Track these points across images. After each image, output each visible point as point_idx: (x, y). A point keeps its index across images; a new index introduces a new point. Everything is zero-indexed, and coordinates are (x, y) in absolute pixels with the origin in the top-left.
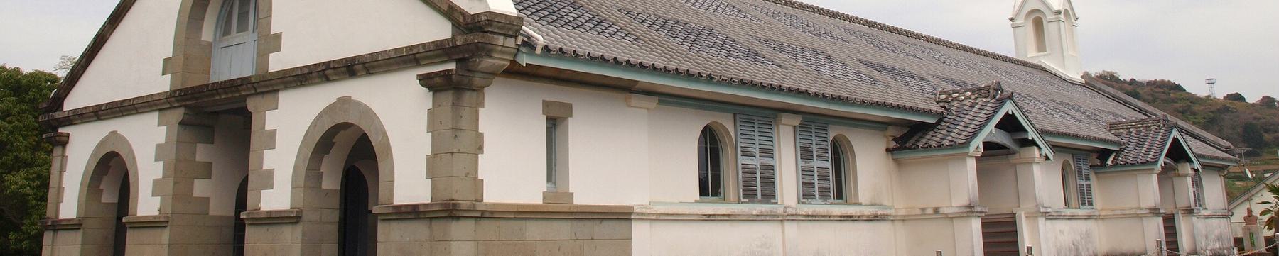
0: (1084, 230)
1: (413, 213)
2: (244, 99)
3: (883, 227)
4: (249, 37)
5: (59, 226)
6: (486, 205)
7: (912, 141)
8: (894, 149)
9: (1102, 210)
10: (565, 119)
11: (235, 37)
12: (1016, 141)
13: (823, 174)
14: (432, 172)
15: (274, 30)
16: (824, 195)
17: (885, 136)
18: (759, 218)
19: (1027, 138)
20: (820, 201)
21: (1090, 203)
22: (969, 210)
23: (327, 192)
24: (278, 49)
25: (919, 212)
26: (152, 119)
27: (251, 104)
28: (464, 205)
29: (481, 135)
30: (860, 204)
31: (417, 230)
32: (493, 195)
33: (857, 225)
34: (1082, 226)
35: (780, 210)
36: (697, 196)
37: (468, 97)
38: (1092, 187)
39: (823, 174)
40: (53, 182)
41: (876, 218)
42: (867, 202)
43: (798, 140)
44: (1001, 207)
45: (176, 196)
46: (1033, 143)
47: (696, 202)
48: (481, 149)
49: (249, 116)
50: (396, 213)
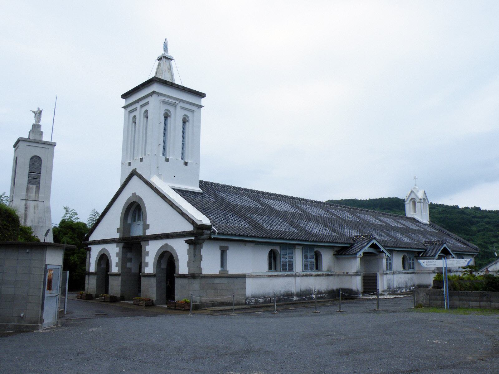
0: (410, 277)
1: (183, 276)
2: (140, 242)
3: (331, 278)
4: (141, 223)
5: (90, 274)
6: (203, 275)
7: (341, 252)
8: (336, 254)
9: (418, 270)
10: (227, 250)
11: (137, 223)
12: (378, 251)
13: (311, 263)
14: (189, 266)
15: (147, 223)
16: (311, 269)
17: (333, 250)
18: (287, 276)
19: (381, 251)
20: (310, 271)
21: (413, 268)
22: (356, 274)
23: (163, 269)
24: (149, 228)
25: (342, 273)
26: (115, 245)
27: (142, 243)
28: (197, 274)
29: (202, 256)
30: (323, 271)
31: (185, 281)
32: (205, 272)
33: (322, 278)
34: (409, 276)
35: (294, 273)
36: (267, 270)
37: (198, 246)
38: (415, 263)
39: (311, 263)
40: (87, 261)
41: (328, 275)
42: (326, 270)
43: (303, 253)
44: (371, 271)
45: (122, 268)
46: (383, 252)
47: (267, 272)
48: (202, 260)
49: (141, 247)
50: (180, 276)
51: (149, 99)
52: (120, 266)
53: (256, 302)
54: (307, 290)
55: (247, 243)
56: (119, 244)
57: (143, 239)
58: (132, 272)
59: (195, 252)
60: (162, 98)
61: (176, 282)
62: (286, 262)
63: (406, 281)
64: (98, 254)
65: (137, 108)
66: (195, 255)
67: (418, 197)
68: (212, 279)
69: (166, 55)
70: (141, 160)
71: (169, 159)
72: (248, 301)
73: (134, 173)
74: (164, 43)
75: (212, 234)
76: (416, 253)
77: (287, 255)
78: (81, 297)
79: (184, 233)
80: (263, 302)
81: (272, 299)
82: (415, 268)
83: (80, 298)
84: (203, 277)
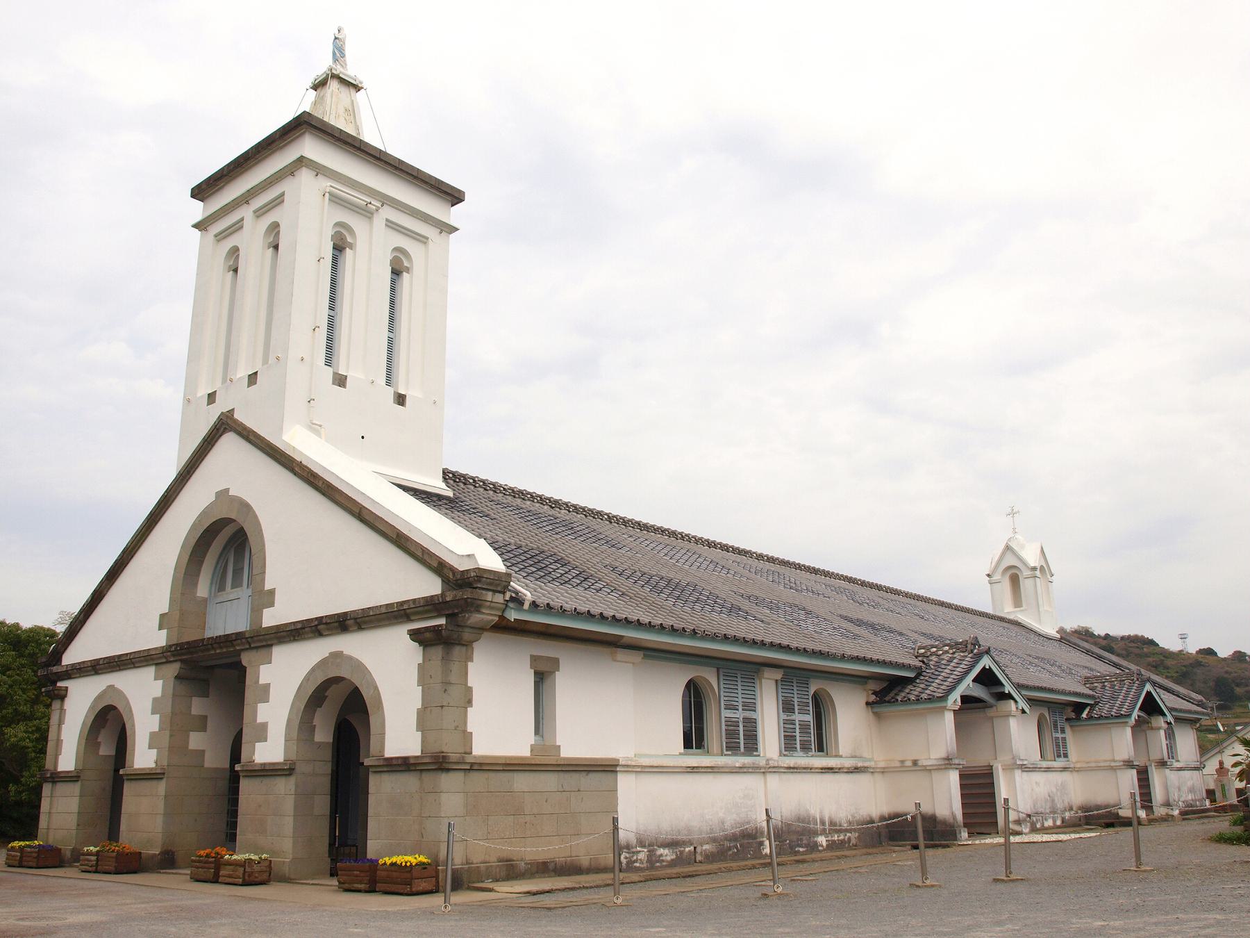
1: (404, 765)
2: (238, 653)
4: (244, 593)
6: (475, 757)
7: (892, 694)
8: (873, 703)
9: (1077, 762)
10: (552, 673)
11: (231, 593)
13: (804, 727)
14: (422, 725)
15: (268, 587)
16: (805, 748)
19: (1004, 692)
21: (1066, 756)
22: (947, 763)
23: (320, 745)
24: (272, 604)
25: (898, 764)
26: (150, 672)
27: (245, 659)
28: (454, 757)
29: (470, 689)
30: (841, 757)
31: (408, 782)
32: (482, 748)
33: (837, 776)
36: (681, 749)
37: (457, 651)
38: (1067, 739)
39: (804, 727)
40: (52, 735)
41: (856, 770)
43: (780, 694)
44: (979, 759)
46: (1010, 696)
47: (681, 754)
48: (470, 702)
49: (243, 670)
50: (387, 766)
51: (286, 186)
53: (652, 859)
54: (799, 819)
55: (619, 649)
56: (164, 667)
57: (250, 644)
58: (207, 765)
59: (446, 671)
60: (326, 184)
61: (372, 789)
63: (1051, 795)
64: (92, 708)
65: (242, 219)
66: (446, 684)
67: (1025, 564)
69: (338, 70)
70: (253, 378)
72: (626, 858)
73: (225, 425)
74: (336, 38)
75: (511, 605)
76: (1069, 709)
78: (21, 860)
79: (405, 607)
80: (672, 860)
81: (699, 850)
82: (1069, 755)
83: (16, 863)
84: (475, 767)
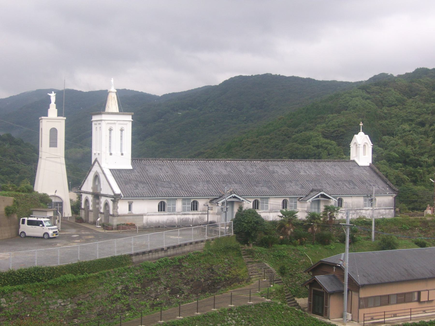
52: (93, 206)
62: (171, 207)
68: (123, 217)
71: (112, 153)
77: (172, 204)
